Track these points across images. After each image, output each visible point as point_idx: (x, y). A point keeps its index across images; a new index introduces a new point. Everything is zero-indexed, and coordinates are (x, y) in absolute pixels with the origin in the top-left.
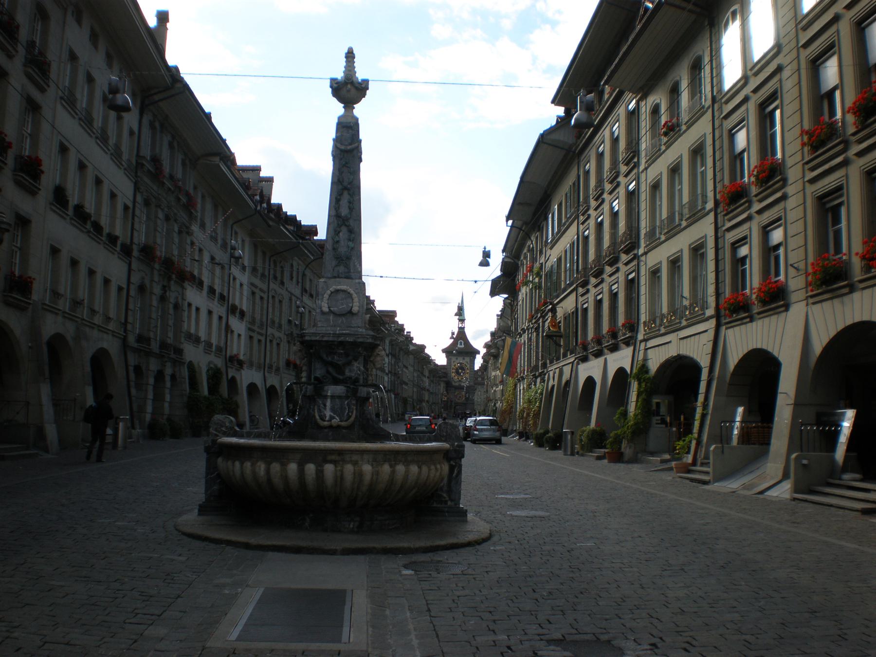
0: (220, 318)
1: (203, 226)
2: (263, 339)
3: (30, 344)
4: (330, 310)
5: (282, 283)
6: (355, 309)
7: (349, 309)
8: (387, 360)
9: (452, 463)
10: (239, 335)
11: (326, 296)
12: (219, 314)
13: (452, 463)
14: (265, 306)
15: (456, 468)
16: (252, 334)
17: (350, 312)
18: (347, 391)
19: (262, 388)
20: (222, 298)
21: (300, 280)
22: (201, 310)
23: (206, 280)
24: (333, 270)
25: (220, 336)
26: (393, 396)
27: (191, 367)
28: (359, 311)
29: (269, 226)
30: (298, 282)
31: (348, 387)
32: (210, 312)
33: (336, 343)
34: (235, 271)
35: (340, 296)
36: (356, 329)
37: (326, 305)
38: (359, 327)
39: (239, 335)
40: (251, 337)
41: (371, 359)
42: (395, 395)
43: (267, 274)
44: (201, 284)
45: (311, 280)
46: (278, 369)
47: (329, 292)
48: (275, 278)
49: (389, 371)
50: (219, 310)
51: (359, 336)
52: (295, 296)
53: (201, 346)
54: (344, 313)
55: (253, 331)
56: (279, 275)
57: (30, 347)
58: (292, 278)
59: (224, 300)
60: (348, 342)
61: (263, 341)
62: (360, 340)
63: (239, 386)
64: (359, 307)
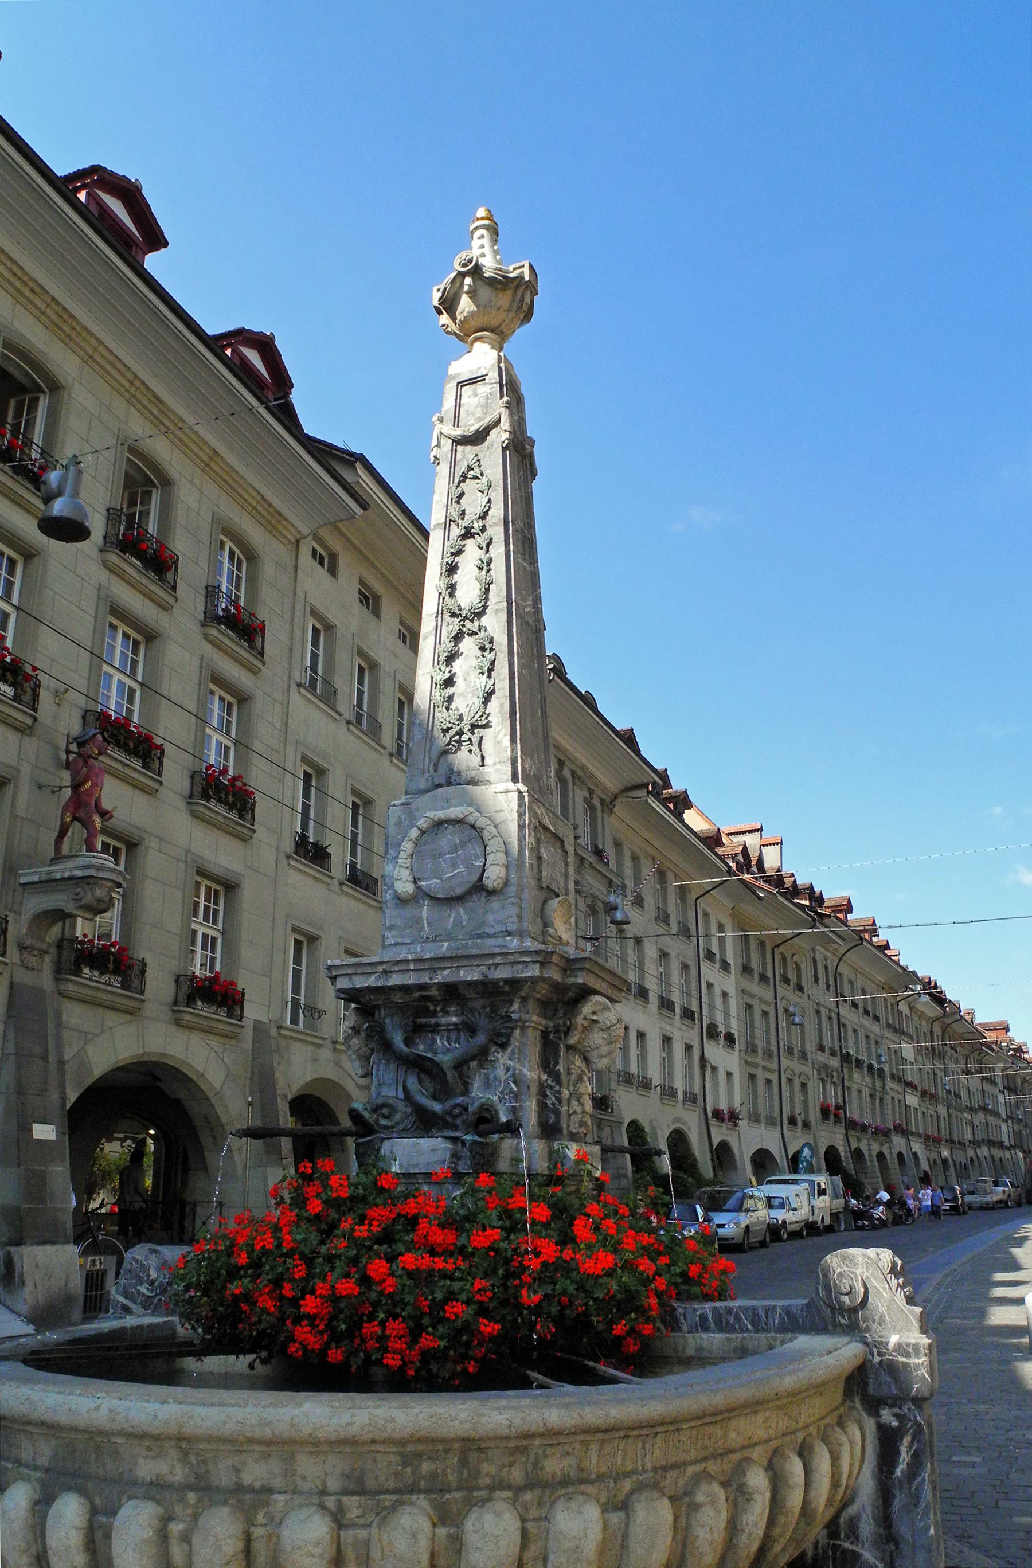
0: (689, 1048)
1: (639, 902)
2: (774, 1077)
3: (250, 1099)
4: (418, 888)
5: (800, 988)
6: (494, 875)
7: (475, 877)
8: (1001, 1099)
9: (886, 1415)
10: (729, 1075)
11: (408, 846)
12: (686, 1040)
13: (886, 1415)
14: (773, 1026)
15: (906, 1440)
16: (753, 1071)
17: (479, 888)
18: (456, 1156)
19: (781, 1157)
20: (688, 1015)
21: (831, 982)
22: (648, 1035)
23: (652, 985)
24: (436, 766)
25: (690, 1076)
26: (1021, 1155)
27: (635, 1129)
28: (506, 883)
29: (760, 898)
30: (828, 987)
31: (454, 1140)
32: (667, 1040)
33: (434, 992)
34: (710, 972)
35: (449, 838)
36: (500, 941)
37: (406, 874)
38: (510, 934)
39: (729, 1075)
40: (752, 1077)
41: (571, 1041)
42: (1024, 1152)
43: (770, 974)
44: (643, 993)
45: (851, 982)
46: (806, 1125)
47: (414, 833)
48: (786, 980)
49: (1007, 1116)
50: (683, 1034)
51: (498, 960)
52: (824, 1006)
53: (655, 1094)
54: (459, 891)
55: (755, 1066)
56: (792, 975)
57: (250, 1104)
58: (816, 980)
59: (693, 1019)
60: (470, 984)
61: (775, 1081)
62: (502, 974)
63: (737, 1158)
64: (507, 867)
